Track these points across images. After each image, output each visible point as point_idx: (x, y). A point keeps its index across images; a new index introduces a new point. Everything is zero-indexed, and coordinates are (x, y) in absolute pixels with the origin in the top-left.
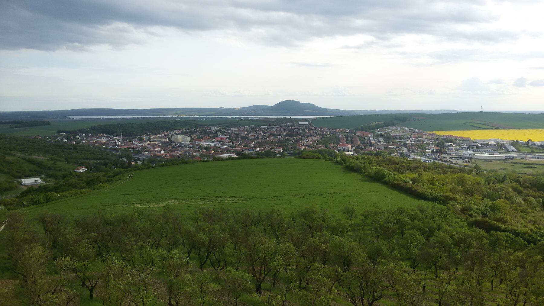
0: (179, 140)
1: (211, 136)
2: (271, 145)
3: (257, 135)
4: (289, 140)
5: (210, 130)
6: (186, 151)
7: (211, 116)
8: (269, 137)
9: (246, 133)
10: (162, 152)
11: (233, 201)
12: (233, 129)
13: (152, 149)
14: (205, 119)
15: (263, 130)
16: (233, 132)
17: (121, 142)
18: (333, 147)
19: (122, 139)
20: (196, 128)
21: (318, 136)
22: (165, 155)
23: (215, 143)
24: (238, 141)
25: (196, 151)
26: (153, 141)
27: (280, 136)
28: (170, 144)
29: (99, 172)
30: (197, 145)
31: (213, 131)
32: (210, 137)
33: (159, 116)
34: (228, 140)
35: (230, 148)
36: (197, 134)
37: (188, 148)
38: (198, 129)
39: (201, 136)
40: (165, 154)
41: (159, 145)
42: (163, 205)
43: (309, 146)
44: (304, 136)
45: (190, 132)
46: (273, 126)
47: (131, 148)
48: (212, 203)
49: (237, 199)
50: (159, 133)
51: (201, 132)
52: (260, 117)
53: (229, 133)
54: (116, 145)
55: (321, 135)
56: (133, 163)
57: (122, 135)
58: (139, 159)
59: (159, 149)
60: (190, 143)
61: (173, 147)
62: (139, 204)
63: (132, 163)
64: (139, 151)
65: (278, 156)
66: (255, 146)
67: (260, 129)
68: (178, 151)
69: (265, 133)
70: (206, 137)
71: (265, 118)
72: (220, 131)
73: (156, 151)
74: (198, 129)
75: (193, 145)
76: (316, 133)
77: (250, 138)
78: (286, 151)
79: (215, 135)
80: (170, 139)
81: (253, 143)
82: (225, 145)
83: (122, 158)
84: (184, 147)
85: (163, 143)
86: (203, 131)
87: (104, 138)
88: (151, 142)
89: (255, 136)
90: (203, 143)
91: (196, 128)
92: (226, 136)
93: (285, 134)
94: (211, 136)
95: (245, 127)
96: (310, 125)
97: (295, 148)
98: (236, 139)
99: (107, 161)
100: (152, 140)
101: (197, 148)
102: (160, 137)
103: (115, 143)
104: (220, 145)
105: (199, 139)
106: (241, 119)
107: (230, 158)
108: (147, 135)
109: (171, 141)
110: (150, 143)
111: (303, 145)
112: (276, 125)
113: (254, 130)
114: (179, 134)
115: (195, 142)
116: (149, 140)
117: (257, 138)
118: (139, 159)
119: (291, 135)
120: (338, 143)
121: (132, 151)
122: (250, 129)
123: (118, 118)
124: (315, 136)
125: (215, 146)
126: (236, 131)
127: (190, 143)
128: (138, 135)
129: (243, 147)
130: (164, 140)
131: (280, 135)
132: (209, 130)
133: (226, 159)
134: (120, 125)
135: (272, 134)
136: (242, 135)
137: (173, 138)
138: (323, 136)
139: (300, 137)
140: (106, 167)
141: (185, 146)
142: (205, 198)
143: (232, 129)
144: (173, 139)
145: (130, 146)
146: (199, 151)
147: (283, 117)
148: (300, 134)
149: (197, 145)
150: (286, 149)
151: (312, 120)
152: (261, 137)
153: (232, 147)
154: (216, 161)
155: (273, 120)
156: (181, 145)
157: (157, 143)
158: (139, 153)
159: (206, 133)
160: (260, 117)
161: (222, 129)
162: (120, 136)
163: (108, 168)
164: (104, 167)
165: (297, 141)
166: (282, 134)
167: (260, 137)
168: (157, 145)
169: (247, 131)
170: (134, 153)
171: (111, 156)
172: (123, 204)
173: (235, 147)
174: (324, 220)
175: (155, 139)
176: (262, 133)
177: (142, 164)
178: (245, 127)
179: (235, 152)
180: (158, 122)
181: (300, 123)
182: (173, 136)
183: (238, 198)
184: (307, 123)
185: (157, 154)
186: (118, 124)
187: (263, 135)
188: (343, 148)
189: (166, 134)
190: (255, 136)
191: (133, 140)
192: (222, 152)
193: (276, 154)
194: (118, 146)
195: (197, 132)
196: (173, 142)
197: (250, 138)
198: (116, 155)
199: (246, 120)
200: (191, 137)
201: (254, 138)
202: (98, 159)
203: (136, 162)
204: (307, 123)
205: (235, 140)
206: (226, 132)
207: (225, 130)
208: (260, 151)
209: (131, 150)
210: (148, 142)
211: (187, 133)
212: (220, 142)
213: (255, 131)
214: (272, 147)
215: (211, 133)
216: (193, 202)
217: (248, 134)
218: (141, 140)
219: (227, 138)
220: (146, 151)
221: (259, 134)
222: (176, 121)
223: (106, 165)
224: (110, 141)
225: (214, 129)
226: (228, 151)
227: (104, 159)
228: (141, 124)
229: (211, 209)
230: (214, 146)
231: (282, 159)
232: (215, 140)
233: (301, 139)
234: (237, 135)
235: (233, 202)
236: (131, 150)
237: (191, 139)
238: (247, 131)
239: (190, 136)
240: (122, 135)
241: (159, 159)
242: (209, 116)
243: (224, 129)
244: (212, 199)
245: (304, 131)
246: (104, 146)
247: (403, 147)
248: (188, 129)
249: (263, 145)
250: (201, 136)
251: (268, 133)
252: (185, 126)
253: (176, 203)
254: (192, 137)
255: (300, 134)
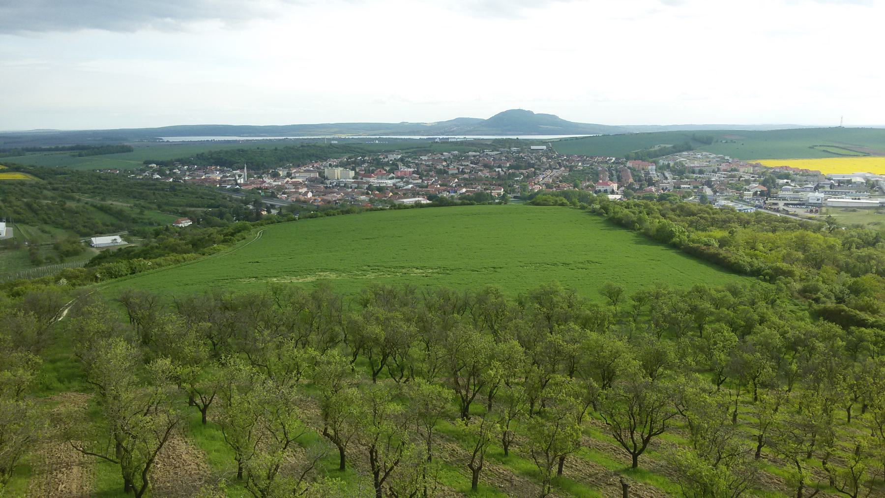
0: (336, 173)
1: (388, 169)
2: (484, 184)
3: (462, 167)
4: (514, 175)
5: (386, 160)
6: (347, 194)
7: (387, 137)
8: (481, 171)
9: (444, 164)
10: (310, 195)
11: (424, 275)
12: (423, 158)
13: (294, 190)
14: (377, 142)
15: (472, 158)
16: (423, 162)
17: (244, 178)
18: (587, 187)
19: (246, 174)
20: (363, 157)
21: (563, 169)
22: (315, 200)
23: (394, 181)
24: (432, 176)
25: (363, 194)
26: (295, 178)
27: (500, 169)
28: (322, 183)
29: (212, 227)
30: (364, 183)
31: (391, 160)
32: (385, 170)
33: (304, 137)
34: (414, 175)
35: (418, 189)
36: (365, 165)
37: (351, 188)
38: (367, 158)
39: (371, 169)
40: (314, 198)
41: (305, 184)
42: (312, 280)
43: (548, 186)
44: (540, 169)
45: (354, 162)
46: (489, 153)
47: (260, 189)
48: (389, 276)
49: (430, 271)
50: (304, 165)
51: (370, 163)
52: (467, 137)
53: (417, 164)
54: (237, 184)
55: (567, 167)
56: (264, 213)
57: (245, 168)
58: (273, 206)
59: (304, 190)
60: (353, 180)
61: (326, 187)
62: (275, 277)
63: (263, 213)
64: (273, 193)
65: (497, 201)
66: (458, 185)
67: (467, 158)
68: (334, 193)
69: (475, 164)
70: (379, 170)
71: (475, 139)
72: (402, 160)
73: (300, 194)
74: (367, 158)
75: (358, 183)
76: (559, 164)
77: (450, 172)
78: (510, 194)
79: (394, 167)
80: (321, 174)
81: (456, 180)
82: (411, 183)
83: (246, 203)
84: (344, 187)
85: (311, 180)
86: (374, 160)
87: (218, 172)
88: (291, 179)
89: (458, 169)
90: (374, 181)
91: (363, 157)
92: (412, 170)
93: (508, 165)
94: (388, 169)
95: (442, 154)
96: (550, 150)
97: (524, 188)
98: (428, 174)
99: (224, 210)
100: (293, 175)
101: (365, 188)
102: (306, 171)
103: (236, 180)
104: (402, 184)
105: (369, 173)
106: (436, 140)
107: (418, 205)
108: (285, 168)
109: (323, 178)
110: (290, 180)
111: (538, 183)
112: (492, 151)
113: (457, 158)
114: (337, 166)
115: (362, 179)
116: (289, 175)
117: (463, 172)
118: (273, 206)
119: (518, 167)
120: (596, 181)
121: (262, 194)
122: (451, 157)
123: (239, 141)
124: (558, 169)
125: (394, 185)
126: (428, 160)
127: (353, 180)
128: (272, 168)
129: (439, 186)
130: (312, 175)
131: (500, 166)
132: (384, 158)
133: (412, 207)
134: (243, 151)
135: (486, 166)
136: (438, 167)
137: (327, 172)
138: (571, 169)
139: (533, 170)
140: (222, 219)
141: (346, 186)
142: (378, 269)
143: (421, 157)
144: (326, 174)
145: (259, 186)
146: (367, 194)
147: (505, 137)
148: (530, 165)
149: (364, 183)
150: (510, 189)
151: (553, 142)
152: (469, 171)
153: (422, 187)
154: (395, 209)
155: (489, 143)
156: (339, 183)
157: (300, 180)
158: (273, 196)
159: (379, 164)
160: (467, 137)
161: (406, 157)
162: (242, 168)
163: (225, 221)
164: (218, 219)
165: (528, 177)
166: (502, 165)
167: (466, 171)
168: (301, 183)
169: (445, 160)
170: (266, 197)
171: (230, 201)
172: (250, 277)
173: (427, 187)
174: (570, 306)
175: (297, 175)
176: (471, 163)
177: (279, 213)
178: (442, 154)
179: (426, 195)
180: (302, 146)
181: (532, 147)
182: (326, 170)
183: (432, 269)
184: (544, 147)
185: (302, 198)
186: (239, 150)
187: (472, 167)
188: (605, 188)
189: (315, 165)
190: (458, 169)
191: (263, 176)
192: (405, 196)
193: (493, 198)
194: (240, 185)
195: (364, 162)
196: (327, 179)
197: (450, 172)
198: (236, 200)
199: (445, 142)
200: (355, 171)
201: (456, 171)
202: (209, 207)
203: (269, 212)
204: (544, 147)
205: (426, 176)
206: (412, 163)
207: (410, 159)
208: (467, 194)
209: (260, 191)
210: (288, 179)
211: (350, 165)
212: (402, 178)
213: (459, 161)
214: (487, 187)
215: (387, 164)
216: (359, 275)
217: (448, 166)
218: (275, 176)
219: (414, 172)
220: (284, 193)
221: (465, 165)
222: (331, 144)
223: (221, 215)
224: (227, 177)
225: (392, 157)
226: (415, 194)
227: (218, 207)
228: (276, 149)
229: (389, 287)
230: (392, 185)
231: (503, 206)
232: (394, 175)
233: (535, 174)
234: (431, 168)
235: (423, 276)
236: (260, 191)
237: (356, 173)
238: (445, 160)
239: (353, 169)
240: (245, 168)
241: (305, 206)
242: (384, 137)
243: (408, 157)
244: (389, 271)
245: (539, 160)
246: (218, 186)
247: (705, 187)
248: (350, 158)
249: (472, 184)
250: (371, 169)
251: (480, 164)
252: (346, 153)
253: (333, 276)
254: (357, 170)
255: (530, 165)
